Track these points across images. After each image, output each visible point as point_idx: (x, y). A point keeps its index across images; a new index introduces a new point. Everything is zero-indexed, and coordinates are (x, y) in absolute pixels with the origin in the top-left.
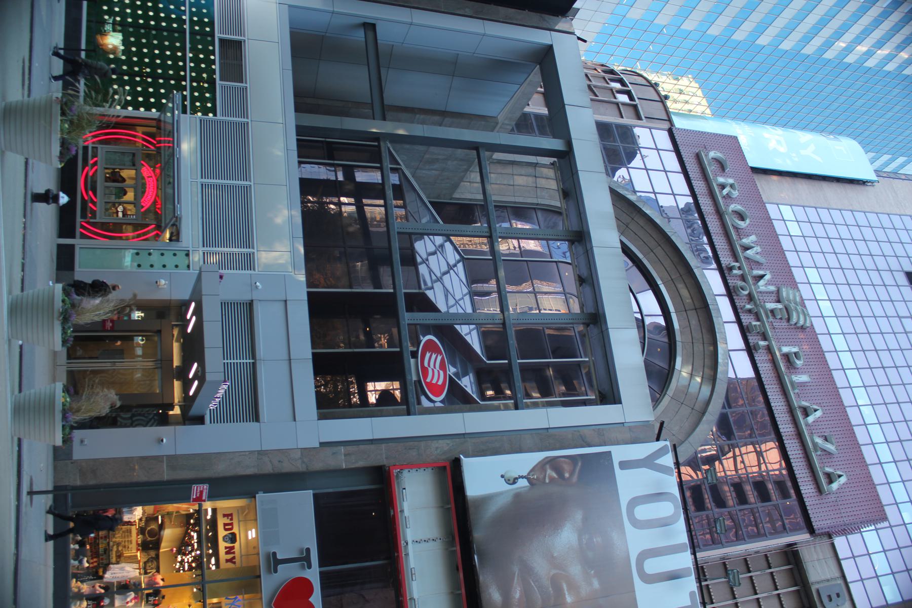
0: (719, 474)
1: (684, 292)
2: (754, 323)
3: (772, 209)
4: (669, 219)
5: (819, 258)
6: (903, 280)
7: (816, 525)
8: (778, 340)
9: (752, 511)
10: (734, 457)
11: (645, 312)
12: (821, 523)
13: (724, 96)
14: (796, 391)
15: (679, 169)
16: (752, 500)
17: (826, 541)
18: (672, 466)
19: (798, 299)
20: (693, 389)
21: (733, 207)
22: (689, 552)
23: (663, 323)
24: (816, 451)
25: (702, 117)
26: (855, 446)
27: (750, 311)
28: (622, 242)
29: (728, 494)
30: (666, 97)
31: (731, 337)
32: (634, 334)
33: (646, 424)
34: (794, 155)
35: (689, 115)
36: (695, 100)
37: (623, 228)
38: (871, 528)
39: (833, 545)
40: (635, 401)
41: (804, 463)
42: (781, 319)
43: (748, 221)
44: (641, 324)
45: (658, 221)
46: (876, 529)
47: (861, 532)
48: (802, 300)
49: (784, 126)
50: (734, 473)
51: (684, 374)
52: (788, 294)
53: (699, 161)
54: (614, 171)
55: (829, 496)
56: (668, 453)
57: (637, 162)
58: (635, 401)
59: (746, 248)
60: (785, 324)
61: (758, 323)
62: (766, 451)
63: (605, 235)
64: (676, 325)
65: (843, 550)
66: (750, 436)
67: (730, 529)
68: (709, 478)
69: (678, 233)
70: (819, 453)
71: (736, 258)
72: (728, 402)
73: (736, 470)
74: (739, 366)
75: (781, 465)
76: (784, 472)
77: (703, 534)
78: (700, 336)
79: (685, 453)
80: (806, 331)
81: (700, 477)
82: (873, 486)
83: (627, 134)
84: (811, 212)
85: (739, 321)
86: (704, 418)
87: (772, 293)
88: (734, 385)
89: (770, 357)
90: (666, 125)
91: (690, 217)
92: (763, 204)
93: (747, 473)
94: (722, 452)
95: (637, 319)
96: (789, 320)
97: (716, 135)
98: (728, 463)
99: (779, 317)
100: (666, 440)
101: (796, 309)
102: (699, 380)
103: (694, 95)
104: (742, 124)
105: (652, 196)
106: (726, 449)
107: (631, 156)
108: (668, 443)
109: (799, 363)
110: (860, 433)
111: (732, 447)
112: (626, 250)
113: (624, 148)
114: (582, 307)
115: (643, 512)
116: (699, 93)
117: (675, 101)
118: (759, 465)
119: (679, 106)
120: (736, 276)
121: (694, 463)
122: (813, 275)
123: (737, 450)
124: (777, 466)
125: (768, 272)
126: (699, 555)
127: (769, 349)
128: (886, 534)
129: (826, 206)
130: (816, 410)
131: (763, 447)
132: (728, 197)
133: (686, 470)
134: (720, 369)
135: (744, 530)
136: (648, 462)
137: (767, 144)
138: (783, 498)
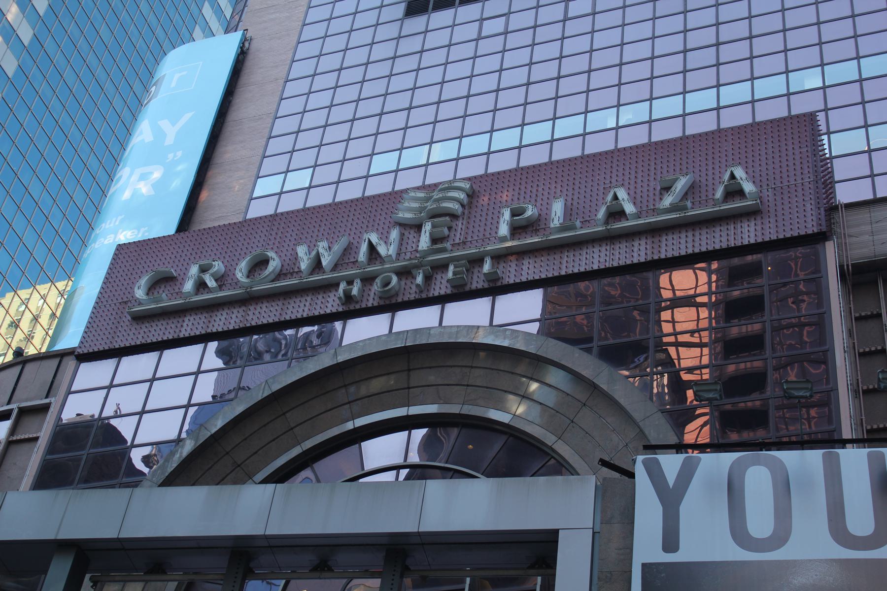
0: (705, 377)
1: (377, 385)
2: (450, 275)
3: (257, 210)
4: (240, 388)
5: (358, 148)
6: (418, 23)
7: (811, 227)
8: (485, 239)
9: (777, 329)
10: (677, 344)
11: (399, 461)
12: (809, 220)
13: (40, 252)
14: (578, 224)
15: (153, 356)
16: (757, 327)
17: (841, 217)
18: (681, 457)
19: (421, 195)
20: (550, 398)
21: (240, 275)
22: (840, 451)
23: (424, 431)
24: (685, 208)
25: (69, 298)
26: (684, 143)
27: (428, 278)
28: (265, 481)
29: (742, 366)
30: (19, 353)
31: (468, 316)
32: (435, 487)
33: (602, 492)
34: (171, 156)
35: (61, 320)
36: (36, 303)
37: (240, 474)
38: (826, 141)
39: (850, 206)
40: (560, 506)
41: (704, 232)
42: (450, 228)
43: (271, 254)
44: (418, 472)
45: (240, 409)
46: (829, 133)
47: (832, 158)
48: (423, 188)
49: (116, 162)
50: (706, 351)
51: (521, 410)
52: (410, 210)
53: (147, 311)
54: (133, 471)
55: (765, 200)
56: (657, 460)
57: (125, 427)
58: (560, 506)
59: (317, 265)
60: (460, 224)
61: (451, 268)
62: (673, 290)
63: (249, 509)
64: (431, 409)
65: (860, 192)
66: (644, 311)
67: (803, 372)
68: (711, 395)
69: (267, 377)
70: (689, 204)
71: (332, 285)
72: (581, 341)
73: (701, 345)
74: (523, 309)
75: (701, 269)
76: (715, 265)
77: (809, 420)
78: (458, 370)
79: (659, 429)
80: (481, 190)
81: (707, 410)
82: (755, 127)
83: (71, 435)
84: (275, 146)
85: (442, 300)
86: (604, 387)
87: (402, 235)
88: (552, 325)
89: (513, 258)
90: (70, 363)
91: (245, 350)
92: (248, 224)
93: (709, 329)
94: (668, 363)
95: (408, 478)
96: (454, 216)
97: (107, 280)
98: (688, 357)
99: (446, 231)
100: (634, 461)
101: (438, 200)
102: (534, 386)
103: (25, 303)
104: (97, 231)
105: (192, 411)
106: (662, 356)
107: (114, 436)
108: (640, 458)
109: (530, 212)
110: (662, 133)
111: (661, 347)
112: (281, 476)
113: (95, 445)
114: (373, 575)
115: (760, 521)
116: (24, 294)
117: (29, 338)
118: (698, 305)
119: (39, 334)
120: (362, 291)
121: (681, 417)
122: (383, 163)
123: (666, 340)
124: (703, 277)
125: (366, 236)
126: (847, 434)
127: (499, 257)
128: (836, 119)
129: (282, 82)
130: (616, 197)
131: (667, 294)
132: (221, 279)
133: (693, 432)
134: (520, 346)
135: (808, 350)
136: (671, 498)
137: (143, 197)
138: (762, 282)
